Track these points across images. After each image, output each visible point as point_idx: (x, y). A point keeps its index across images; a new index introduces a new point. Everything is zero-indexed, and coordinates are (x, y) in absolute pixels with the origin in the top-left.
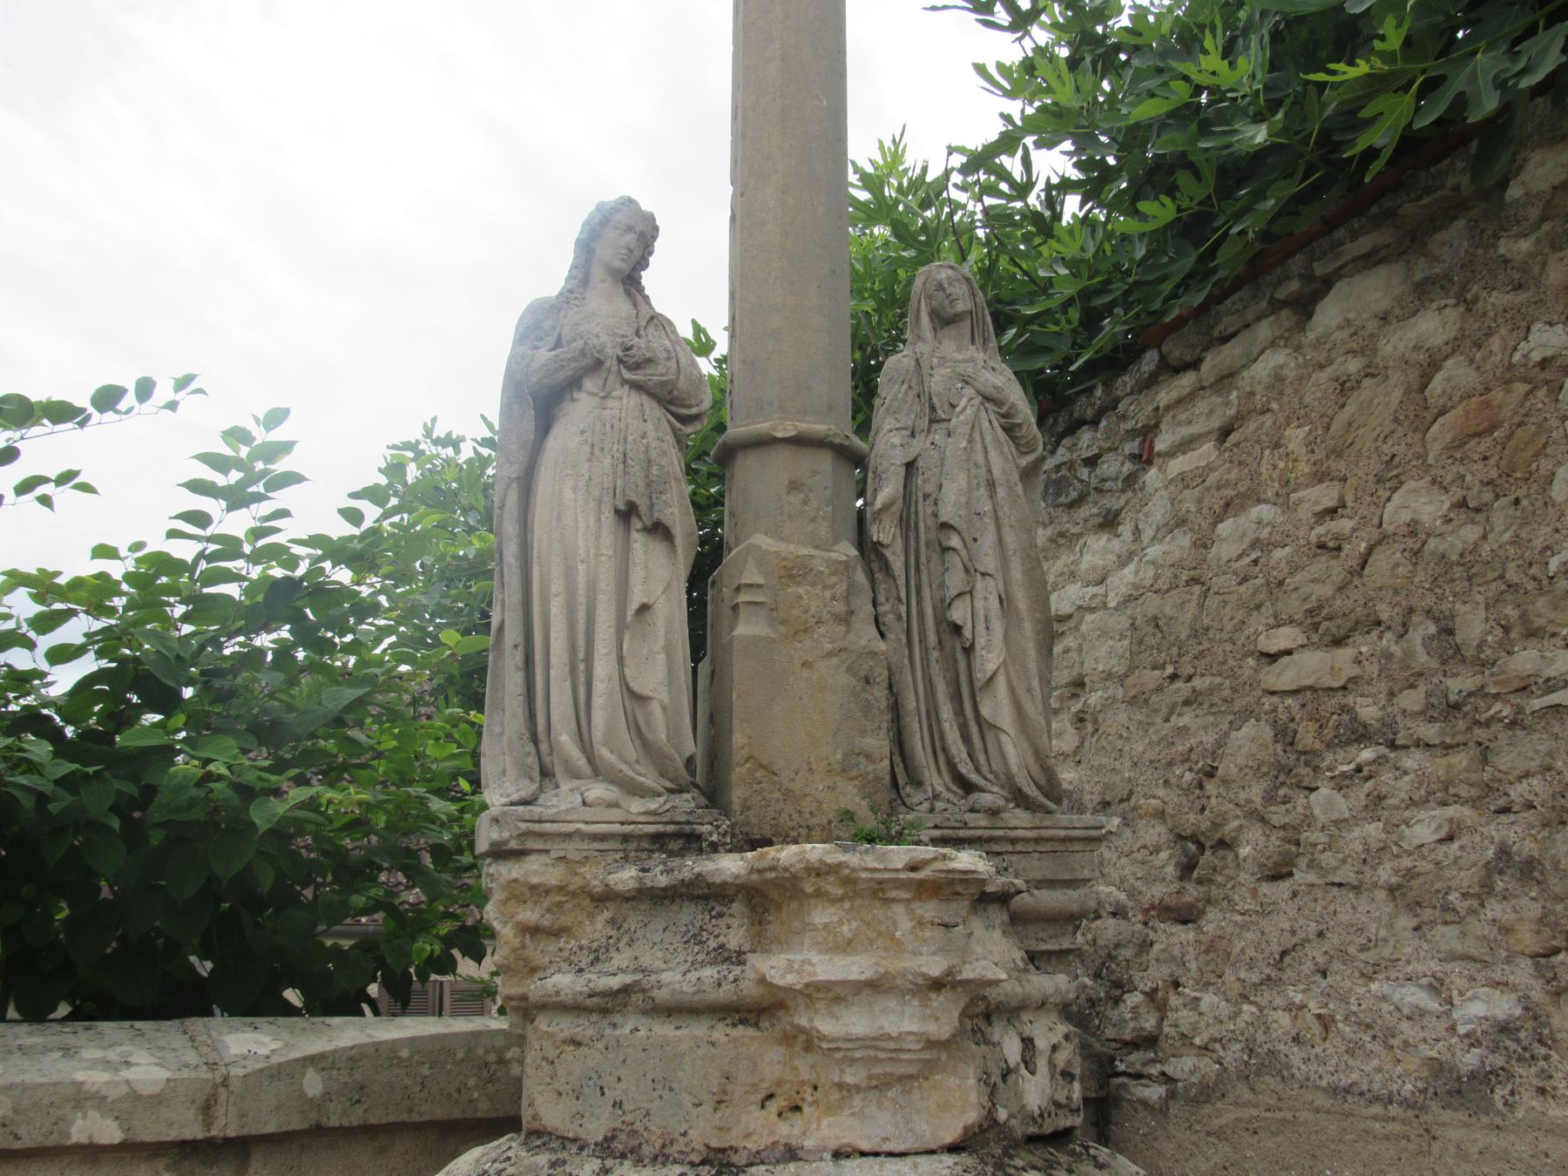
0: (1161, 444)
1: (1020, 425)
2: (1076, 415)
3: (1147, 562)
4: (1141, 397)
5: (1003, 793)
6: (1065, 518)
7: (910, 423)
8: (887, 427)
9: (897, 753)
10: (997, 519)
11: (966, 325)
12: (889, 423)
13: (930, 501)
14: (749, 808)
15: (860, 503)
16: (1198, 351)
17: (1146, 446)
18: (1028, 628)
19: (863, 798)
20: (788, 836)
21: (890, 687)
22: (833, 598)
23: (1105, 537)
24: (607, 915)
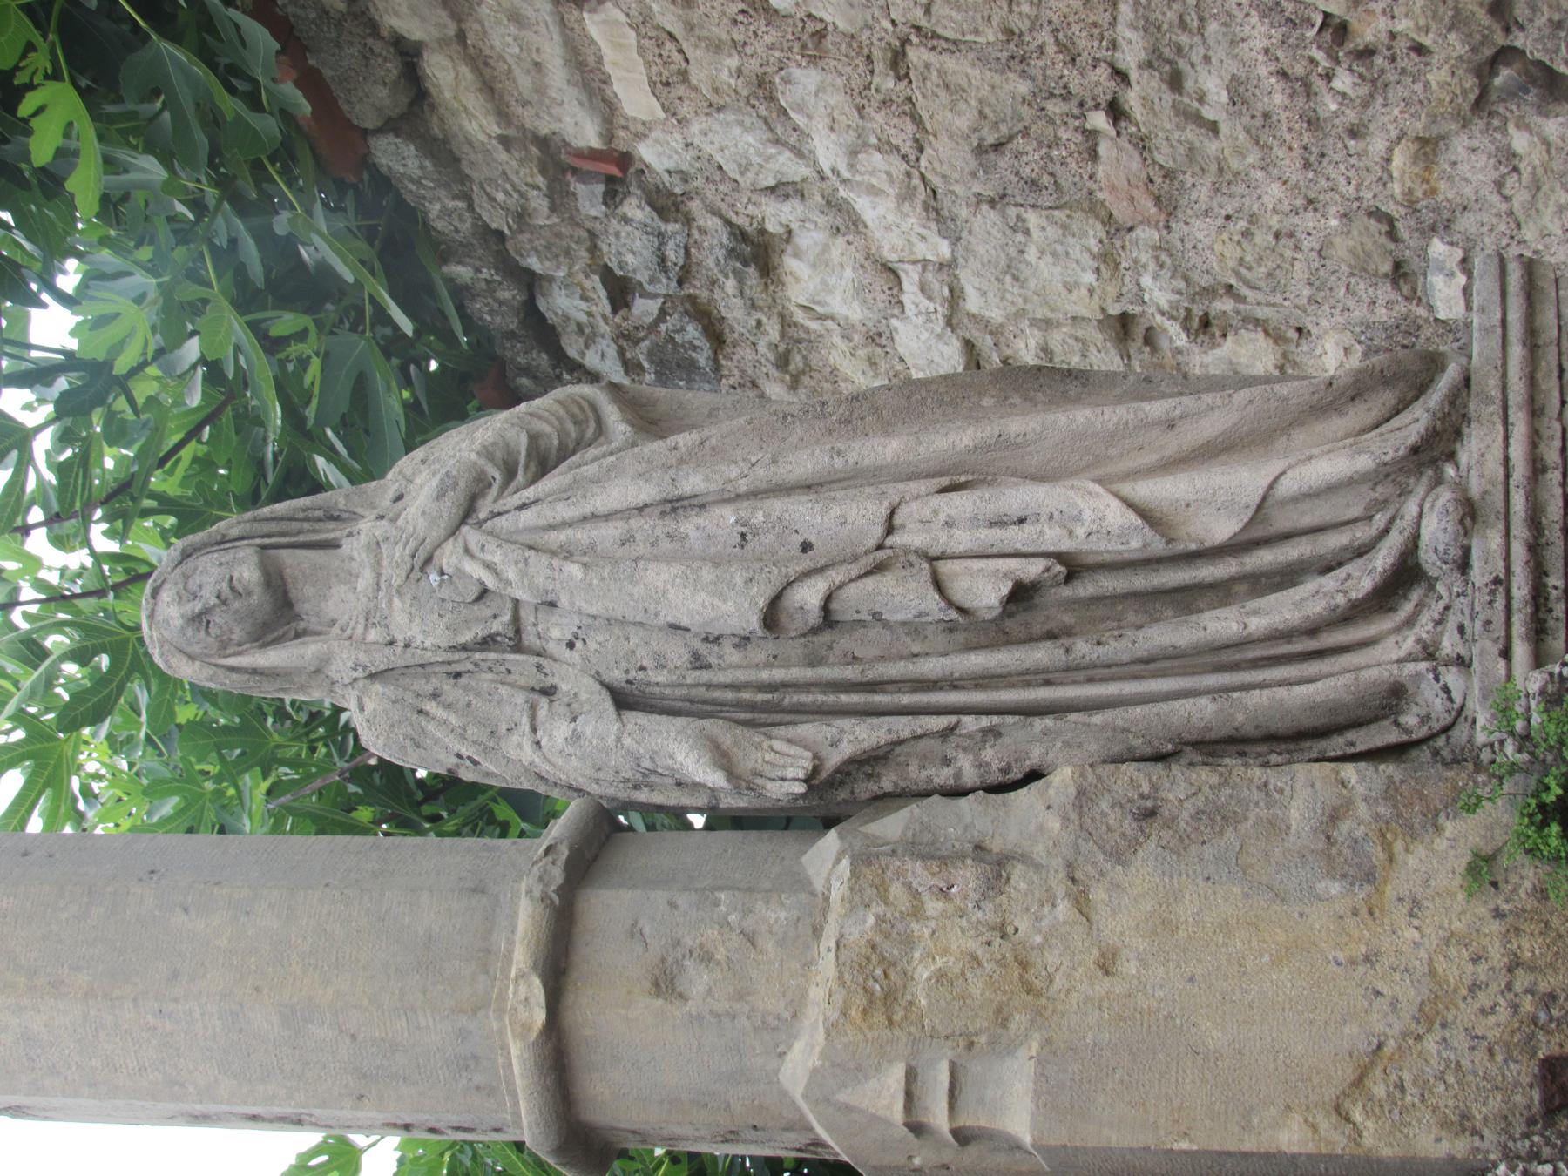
0: (585, 133)
1: (534, 438)
2: (513, 324)
3: (851, 166)
4: (474, 175)
5: (1421, 490)
6: (745, 353)
7: (520, 698)
8: (528, 754)
9: (1318, 746)
10: (755, 494)
11: (294, 562)
12: (520, 748)
13: (709, 653)
14: (1465, 1116)
15: (698, 821)
16: (377, 46)
17: (587, 166)
18: (1019, 425)
19: (1438, 829)
20: (1534, 1020)
21: (1160, 758)
22: (944, 893)
23: (790, 263)
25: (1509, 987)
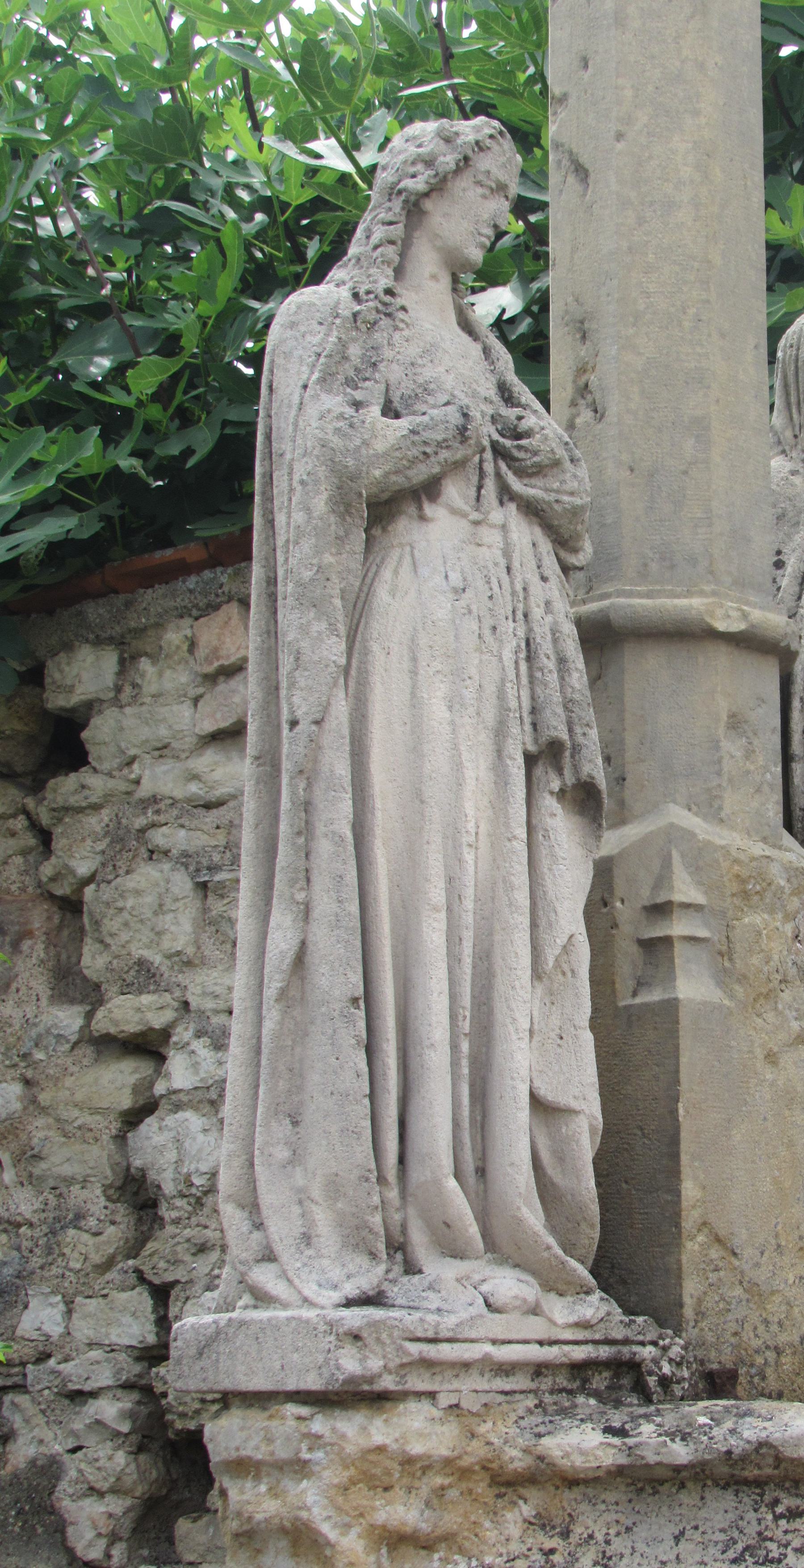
24: (527, 1510)
25: (768, 1347)
